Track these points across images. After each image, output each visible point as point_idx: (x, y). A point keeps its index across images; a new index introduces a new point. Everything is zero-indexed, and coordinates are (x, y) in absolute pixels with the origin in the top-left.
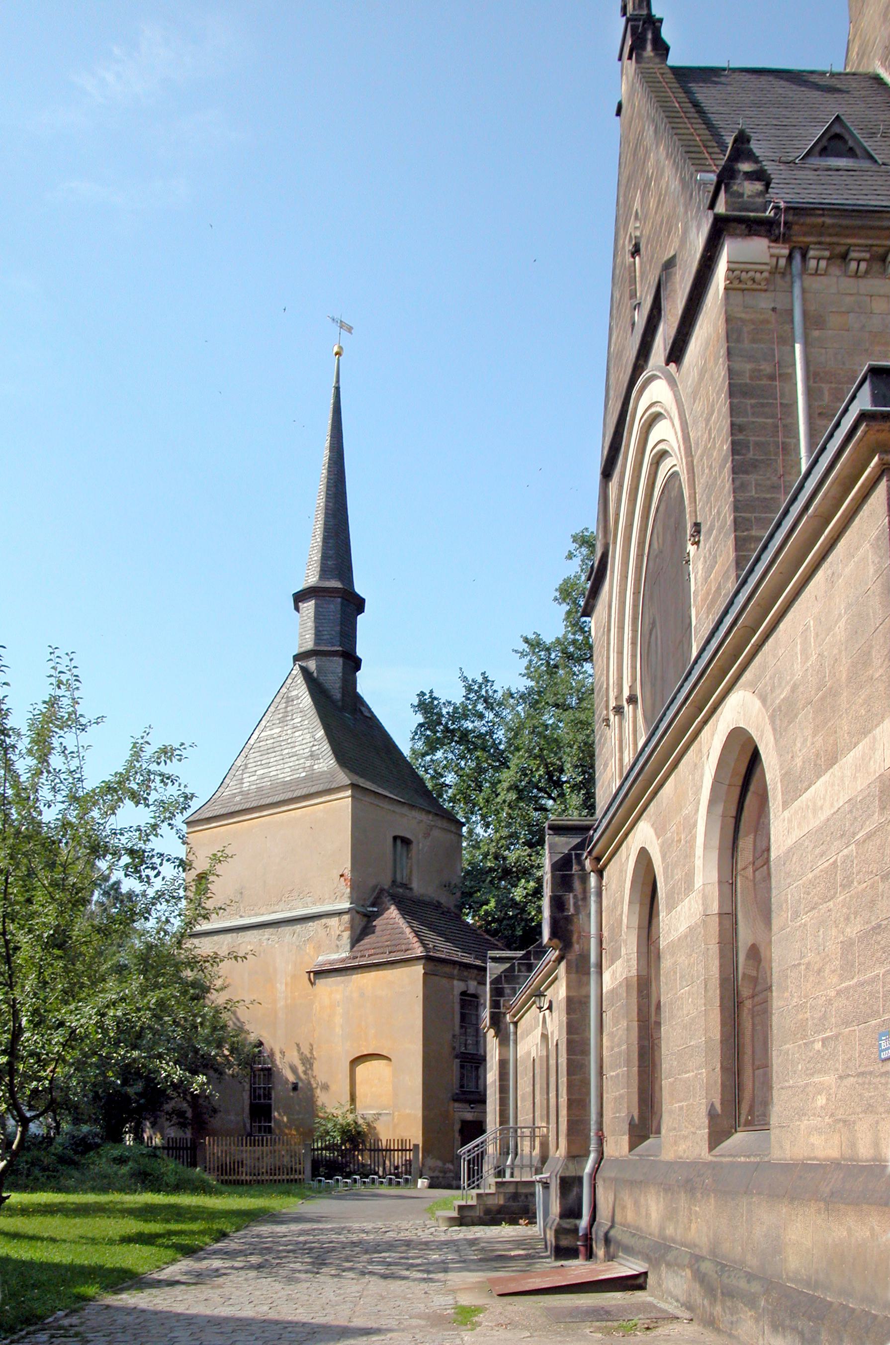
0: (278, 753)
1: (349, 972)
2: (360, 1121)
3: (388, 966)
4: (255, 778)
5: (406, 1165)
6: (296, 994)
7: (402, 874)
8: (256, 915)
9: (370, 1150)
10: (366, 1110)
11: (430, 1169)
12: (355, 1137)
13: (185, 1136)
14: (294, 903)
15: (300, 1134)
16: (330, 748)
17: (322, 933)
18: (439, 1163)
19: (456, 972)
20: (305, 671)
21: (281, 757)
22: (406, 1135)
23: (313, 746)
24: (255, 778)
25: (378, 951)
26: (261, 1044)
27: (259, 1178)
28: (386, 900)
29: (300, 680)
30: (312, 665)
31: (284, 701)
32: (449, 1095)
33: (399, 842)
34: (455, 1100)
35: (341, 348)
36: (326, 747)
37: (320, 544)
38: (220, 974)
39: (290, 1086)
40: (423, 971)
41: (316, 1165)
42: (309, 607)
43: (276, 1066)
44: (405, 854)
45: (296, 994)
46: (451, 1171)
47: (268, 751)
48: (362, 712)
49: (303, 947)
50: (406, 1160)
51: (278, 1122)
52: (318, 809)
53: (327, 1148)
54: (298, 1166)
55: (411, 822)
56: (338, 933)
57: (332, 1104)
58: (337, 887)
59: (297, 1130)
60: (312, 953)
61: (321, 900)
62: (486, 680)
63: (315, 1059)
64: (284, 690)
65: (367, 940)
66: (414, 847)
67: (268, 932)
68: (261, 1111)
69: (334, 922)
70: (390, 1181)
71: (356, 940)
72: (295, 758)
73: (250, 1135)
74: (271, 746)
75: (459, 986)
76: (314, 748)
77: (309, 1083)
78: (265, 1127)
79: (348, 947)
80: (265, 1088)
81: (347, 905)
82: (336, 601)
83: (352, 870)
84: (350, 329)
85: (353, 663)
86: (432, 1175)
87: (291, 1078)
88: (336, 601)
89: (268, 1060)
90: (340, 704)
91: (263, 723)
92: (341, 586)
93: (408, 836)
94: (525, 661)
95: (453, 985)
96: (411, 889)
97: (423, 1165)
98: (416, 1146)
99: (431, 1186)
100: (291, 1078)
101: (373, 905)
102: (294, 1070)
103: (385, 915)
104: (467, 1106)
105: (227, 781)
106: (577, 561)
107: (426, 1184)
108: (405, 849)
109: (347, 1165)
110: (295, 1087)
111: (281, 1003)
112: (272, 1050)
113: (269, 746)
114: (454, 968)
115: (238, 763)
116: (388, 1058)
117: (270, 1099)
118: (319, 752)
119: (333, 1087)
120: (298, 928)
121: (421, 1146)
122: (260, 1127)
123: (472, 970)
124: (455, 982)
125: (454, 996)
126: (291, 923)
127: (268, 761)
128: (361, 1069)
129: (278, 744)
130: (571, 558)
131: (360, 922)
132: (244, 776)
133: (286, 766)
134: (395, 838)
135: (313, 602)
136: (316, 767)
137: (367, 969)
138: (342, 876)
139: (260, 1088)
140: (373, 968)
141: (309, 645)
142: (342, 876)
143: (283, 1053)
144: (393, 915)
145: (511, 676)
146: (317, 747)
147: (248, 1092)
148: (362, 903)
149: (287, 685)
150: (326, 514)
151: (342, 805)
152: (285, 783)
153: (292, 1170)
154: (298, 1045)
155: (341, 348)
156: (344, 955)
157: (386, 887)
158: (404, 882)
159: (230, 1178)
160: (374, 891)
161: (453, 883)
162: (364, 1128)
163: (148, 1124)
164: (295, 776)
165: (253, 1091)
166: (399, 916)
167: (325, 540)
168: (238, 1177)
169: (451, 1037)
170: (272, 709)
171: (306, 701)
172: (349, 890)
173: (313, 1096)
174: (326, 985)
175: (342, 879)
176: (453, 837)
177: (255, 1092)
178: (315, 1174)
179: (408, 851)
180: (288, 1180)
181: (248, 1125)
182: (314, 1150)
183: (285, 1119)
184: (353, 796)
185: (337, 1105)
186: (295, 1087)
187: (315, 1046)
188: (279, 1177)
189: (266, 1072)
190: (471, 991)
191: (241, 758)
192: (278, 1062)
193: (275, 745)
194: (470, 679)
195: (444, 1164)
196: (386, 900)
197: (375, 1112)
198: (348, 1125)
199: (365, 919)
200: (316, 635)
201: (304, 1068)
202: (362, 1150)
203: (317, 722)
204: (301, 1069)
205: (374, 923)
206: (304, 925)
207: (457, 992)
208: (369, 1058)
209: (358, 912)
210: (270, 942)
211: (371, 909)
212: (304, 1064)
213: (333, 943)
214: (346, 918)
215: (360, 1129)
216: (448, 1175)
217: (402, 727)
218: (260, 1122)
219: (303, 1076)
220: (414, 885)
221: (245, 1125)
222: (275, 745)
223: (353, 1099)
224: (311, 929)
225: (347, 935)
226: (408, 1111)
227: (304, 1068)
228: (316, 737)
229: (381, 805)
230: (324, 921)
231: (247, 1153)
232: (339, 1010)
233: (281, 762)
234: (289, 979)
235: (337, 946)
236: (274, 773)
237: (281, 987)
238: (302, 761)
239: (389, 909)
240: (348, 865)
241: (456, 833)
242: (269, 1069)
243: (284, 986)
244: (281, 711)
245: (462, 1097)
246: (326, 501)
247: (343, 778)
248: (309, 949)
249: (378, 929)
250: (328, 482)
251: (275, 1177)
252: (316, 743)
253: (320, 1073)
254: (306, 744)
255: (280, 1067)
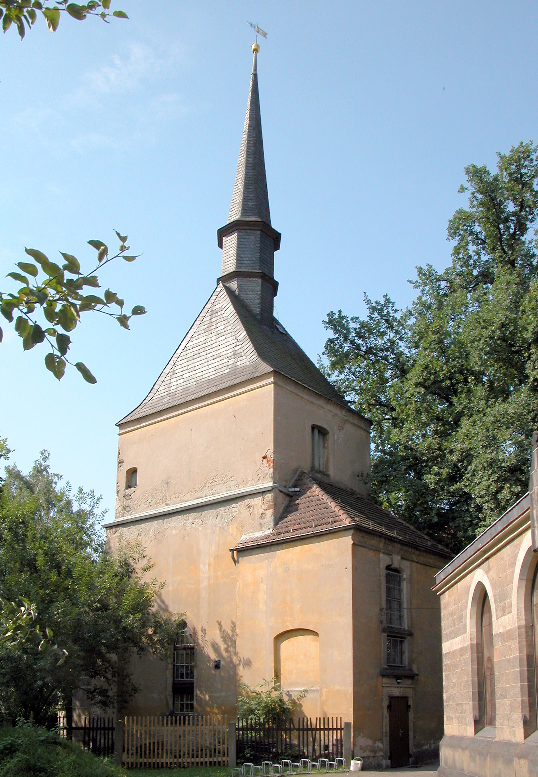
0: (203, 358)
1: (273, 548)
2: (286, 699)
3: (315, 539)
4: (182, 381)
5: (337, 745)
6: (219, 573)
7: (319, 460)
8: (181, 502)
9: (299, 730)
10: (292, 686)
11: (361, 749)
12: (281, 716)
13: (103, 715)
14: (218, 487)
15: (223, 713)
16: (252, 345)
17: (245, 513)
18: (370, 742)
19: (381, 545)
20: (230, 292)
21: (206, 360)
22: (332, 713)
23: (236, 346)
24: (182, 381)
25: (302, 525)
26: (183, 624)
27: (180, 760)
28: (307, 481)
29: (224, 294)
30: (234, 285)
31: (208, 314)
32: (378, 670)
33: (316, 432)
34: (383, 676)
35: (257, 45)
36: (249, 345)
37: (242, 190)
38: (145, 554)
39: (212, 665)
40: (352, 542)
41: (240, 746)
42: (231, 241)
43: (198, 644)
44: (321, 444)
45: (219, 573)
46: (380, 750)
47: (194, 357)
48: (277, 329)
49: (226, 528)
50: (337, 740)
51: (200, 701)
52: (241, 400)
53: (252, 729)
54: (221, 747)
55: (325, 414)
56: (261, 511)
57: (255, 681)
58: (260, 469)
59: (219, 708)
60: (235, 533)
61: (244, 482)
62: (388, 301)
63: (237, 635)
64: (209, 305)
65: (290, 518)
66: (330, 437)
67: (192, 516)
68: (183, 689)
69: (257, 501)
70: (323, 764)
71: (278, 519)
72: (219, 359)
73: (172, 714)
74: (197, 352)
75: (384, 560)
76: (237, 348)
77: (231, 662)
78: (187, 704)
79: (272, 524)
80: (187, 667)
81: (269, 484)
82: (256, 233)
83: (275, 452)
84: (265, 35)
85: (271, 287)
86: (365, 755)
87: (213, 656)
88: (256, 233)
89: (191, 640)
90: (259, 317)
91: (190, 335)
92: (259, 219)
93: (325, 426)
94: (417, 292)
95: (379, 559)
96: (328, 476)
97: (354, 745)
98: (348, 724)
99: (364, 768)
100: (213, 656)
101: (295, 486)
102: (216, 648)
103: (308, 494)
104: (394, 681)
105: (156, 387)
106: (467, 195)
107: (359, 766)
108: (321, 441)
109: (274, 745)
110: (217, 666)
111: (205, 584)
112: (194, 629)
113: (195, 353)
114: (380, 542)
115: (167, 371)
116: (315, 633)
117: (193, 677)
118: (241, 350)
119: (256, 664)
120: (221, 510)
121: (352, 724)
122: (182, 705)
123: (396, 545)
124: (381, 555)
125: (380, 568)
126: (215, 506)
127: (194, 365)
128: (286, 646)
129: (203, 350)
130: (463, 191)
131: (283, 501)
132: (172, 381)
133: (210, 366)
134: (314, 427)
135: (236, 234)
136: (239, 363)
137: (292, 544)
138: (264, 458)
139: (182, 666)
140: (298, 543)
141: (231, 267)
142: (264, 458)
143: (204, 631)
144: (317, 493)
145: (406, 299)
146: (240, 347)
147: (171, 671)
148: (284, 484)
149: (212, 301)
150: (247, 166)
151: (266, 391)
152: (209, 381)
153: (215, 751)
154: (220, 624)
155: (257, 45)
156: (268, 532)
157: (306, 471)
158: (321, 469)
159: (150, 760)
160: (295, 474)
161: (365, 474)
162: (288, 705)
163: (78, 703)
164: (219, 374)
165: (176, 669)
166: (322, 493)
167: (247, 186)
168: (158, 760)
169: (378, 610)
170: (198, 322)
171: (230, 310)
172: (272, 470)
173: (236, 674)
174: (250, 563)
175: (265, 460)
176: (363, 433)
177: (177, 670)
178: (241, 758)
179: (325, 441)
180: (210, 763)
181: (171, 703)
182: (238, 729)
183: (207, 697)
184: (275, 383)
185: (262, 682)
186: (217, 666)
187: (237, 624)
188: (202, 760)
189: (189, 651)
190: (395, 565)
191: (169, 366)
192: (200, 642)
193: (200, 351)
194: (373, 301)
195: (375, 743)
196: (307, 481)
197: (302, 689)
198: (273, 701)
199: (288, 499)
200: (237, 260)
201: (225, 646)
202: (290, 730)
203: (240, 326)
204: (223, 646)
205: (297, 502)
206: (227, 507)
207: (383, 566)
208: (294, 633)
209: (281, 491)
210: (194, 525)
211: (293, 490)
212: (225, 641)
213: (256, 521)
214: (270, 496)
215: (285, 706)
216: (377, 754)
217: (313, 342)
218: (182, 700)
219: (225, 654)
220: (331, 472)
221: (167, 703)
222: (200, 351)
223: (277, 675)
224: (234, 510)
225: (270, 513)
226: (337, 687)
227: (225, 646)
228: (239, 338)
229: (301, 395)
230: (247, 501)
231: (168, 732)
232: (263, 586)
233: (206, 364)
234: (212, 559)
235: (261, 524)
236: (200, 374)
237: (204, 568)
238: (226, 360)
239: (311, 488)
240: (271, 447)
241: (364, 430)
242: (192, 648)
243: (207, 567)
244: (206, 323)
245: (389, 672)
246: (247, 157)
247: (267, 368)
248: (232, 529)
249: (300, 506)
250: (248, 143)
251: (197, 760)
252: (238, 343)
253: (244, 650)
254: (231, 345)
255: (202, 645)
